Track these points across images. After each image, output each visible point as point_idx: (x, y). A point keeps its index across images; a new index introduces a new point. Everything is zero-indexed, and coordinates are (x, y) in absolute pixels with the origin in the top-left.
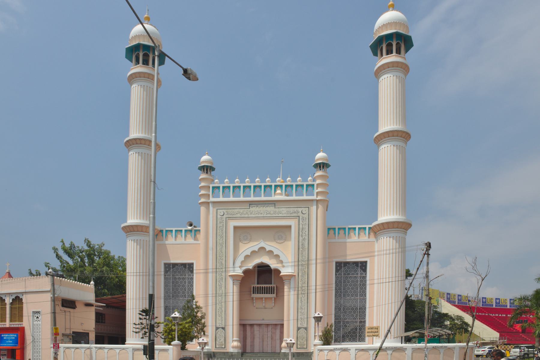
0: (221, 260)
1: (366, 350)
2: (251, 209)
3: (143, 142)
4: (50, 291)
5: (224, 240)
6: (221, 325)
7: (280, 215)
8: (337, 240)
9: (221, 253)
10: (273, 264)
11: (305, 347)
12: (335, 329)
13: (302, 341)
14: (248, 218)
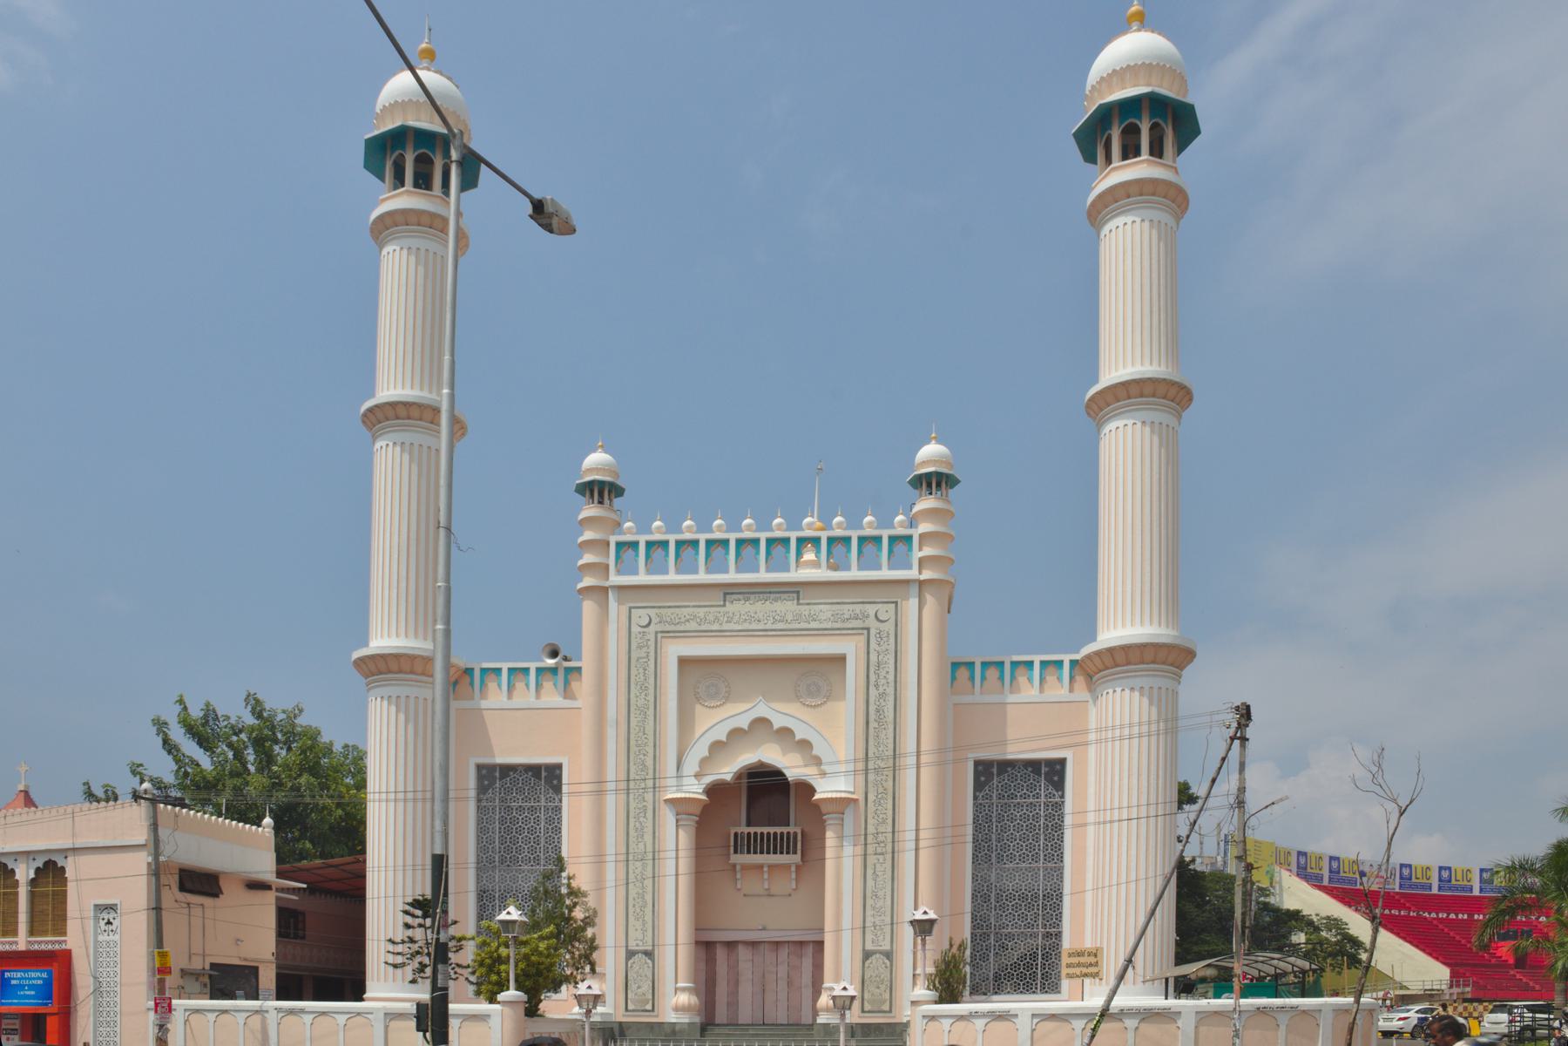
0: (641, 756)
1: (1063, 1017)
2: (730, 608)
3: (415, 412)
4: (145, 845)
5: (651, 698)
6: (641, 944)
7: (814, 625)
8: (977, 697)
9: (641, 734)
10: (793, 767)
11: (886, 1007)
12: (973, 956)
13: (877, 990)
14: (721, 634)
